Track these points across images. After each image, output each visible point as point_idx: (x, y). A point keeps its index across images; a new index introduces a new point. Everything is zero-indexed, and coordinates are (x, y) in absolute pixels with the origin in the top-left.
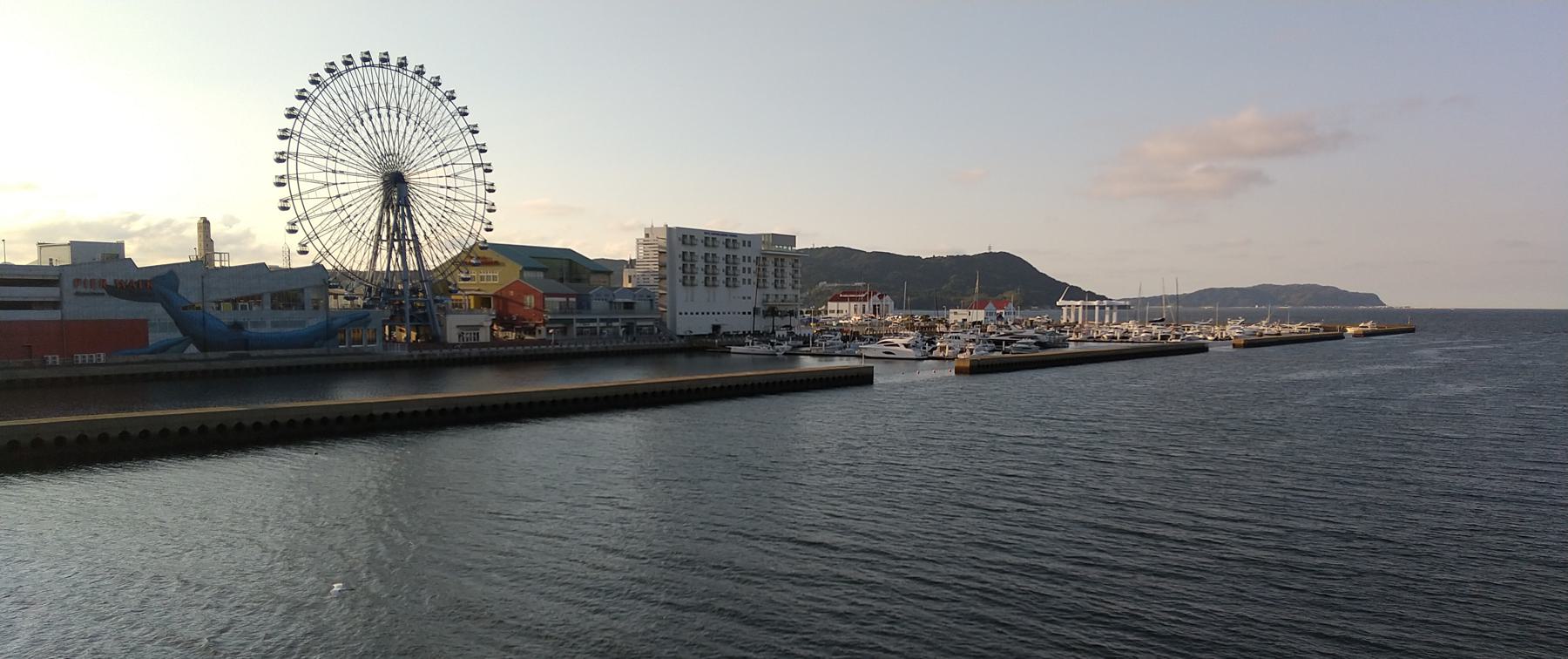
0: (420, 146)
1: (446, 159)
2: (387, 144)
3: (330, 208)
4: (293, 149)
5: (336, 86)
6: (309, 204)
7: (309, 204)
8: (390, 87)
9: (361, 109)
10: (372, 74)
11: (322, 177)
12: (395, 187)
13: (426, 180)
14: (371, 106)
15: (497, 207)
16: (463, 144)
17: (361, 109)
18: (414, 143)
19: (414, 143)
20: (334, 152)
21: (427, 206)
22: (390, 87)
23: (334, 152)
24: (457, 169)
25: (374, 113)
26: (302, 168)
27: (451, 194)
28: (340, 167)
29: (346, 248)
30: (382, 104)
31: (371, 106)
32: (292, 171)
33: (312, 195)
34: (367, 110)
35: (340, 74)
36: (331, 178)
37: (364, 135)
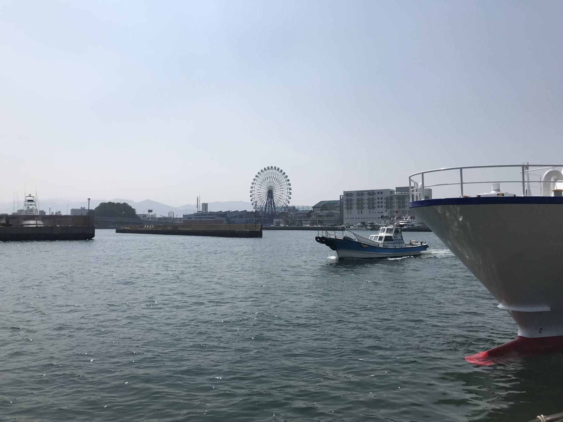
0: (277, 186)
1: (282, 190)
2: (272, 185)
3: (257, 194)
4: (255, 182)
5: (268, 171)
6: (287, 191)
7: (255, 193)
8: (277, 175)
9: (270, 177)
10: (274, 171)
11: (283, 195)
12: (270, 193)
13: (277, 194)
14: (272, 177)
15: (290, 202)
16: (286, 187)
17: (270, 177)
18: (276, 185)
19: (276, 185)
20: (280, 199)
21: (265, 185)
22: (277, 175)
23: (280, 199)
24: (283, 192)
25: (272, 178)
26: (286, 197)
27: (260, 186)
28: (279, 196)
29: (283, 181)
30: (274, 177)
31: (272, 177)
32: (254, 186)
33: (285, 192)
34: (271, 177)
35: (269, 169)
36: (281, 195)
37: (267, 182)
